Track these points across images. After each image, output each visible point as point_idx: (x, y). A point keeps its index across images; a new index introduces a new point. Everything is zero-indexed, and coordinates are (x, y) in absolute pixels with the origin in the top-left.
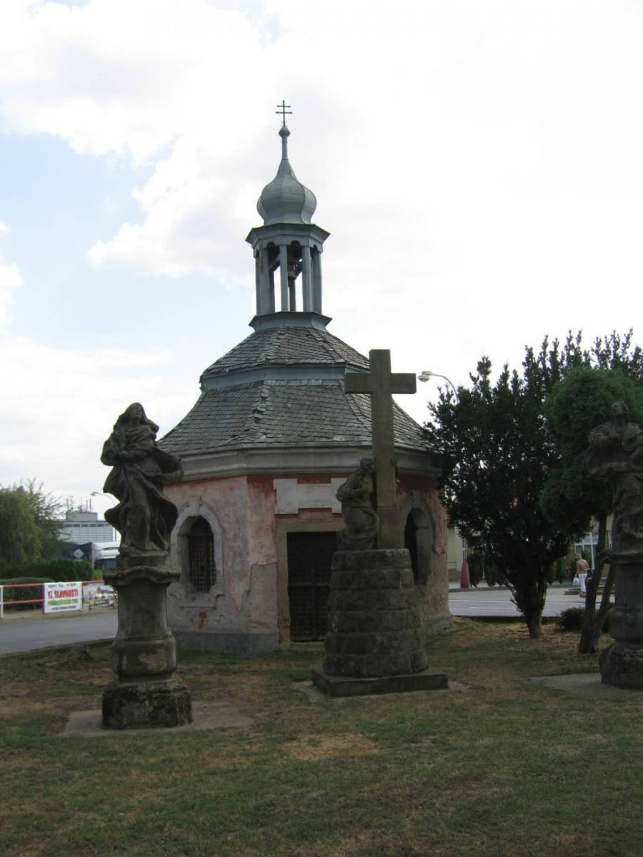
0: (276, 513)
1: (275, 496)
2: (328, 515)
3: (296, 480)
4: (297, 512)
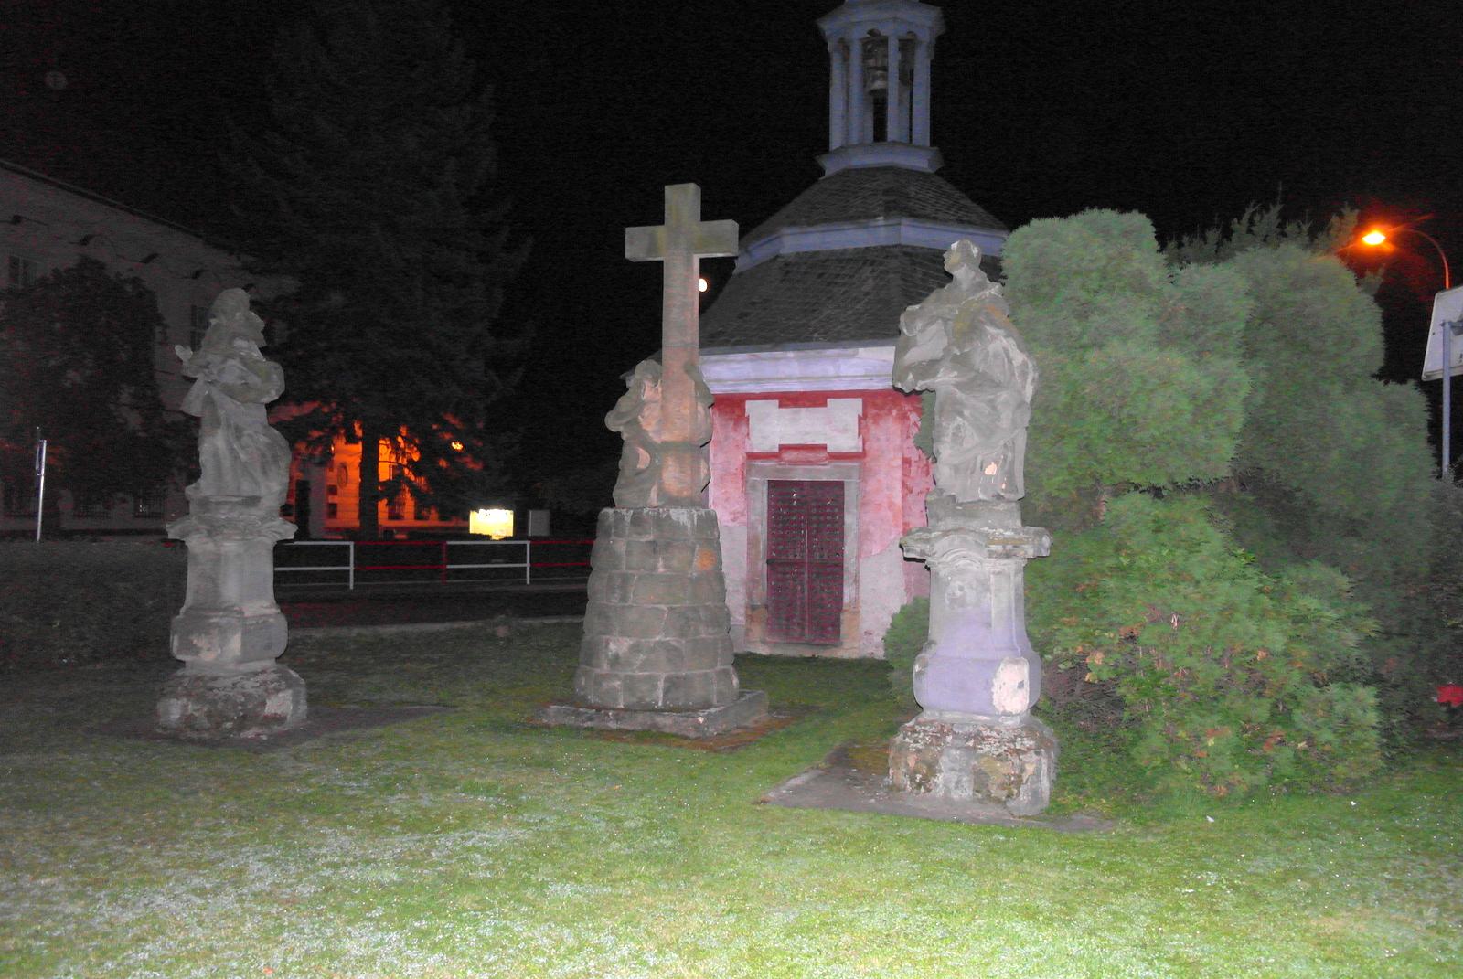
0: (749, 450)
1: (748, 425)
2: (822, 455)
3: (777, 402)
4: (776, 450)
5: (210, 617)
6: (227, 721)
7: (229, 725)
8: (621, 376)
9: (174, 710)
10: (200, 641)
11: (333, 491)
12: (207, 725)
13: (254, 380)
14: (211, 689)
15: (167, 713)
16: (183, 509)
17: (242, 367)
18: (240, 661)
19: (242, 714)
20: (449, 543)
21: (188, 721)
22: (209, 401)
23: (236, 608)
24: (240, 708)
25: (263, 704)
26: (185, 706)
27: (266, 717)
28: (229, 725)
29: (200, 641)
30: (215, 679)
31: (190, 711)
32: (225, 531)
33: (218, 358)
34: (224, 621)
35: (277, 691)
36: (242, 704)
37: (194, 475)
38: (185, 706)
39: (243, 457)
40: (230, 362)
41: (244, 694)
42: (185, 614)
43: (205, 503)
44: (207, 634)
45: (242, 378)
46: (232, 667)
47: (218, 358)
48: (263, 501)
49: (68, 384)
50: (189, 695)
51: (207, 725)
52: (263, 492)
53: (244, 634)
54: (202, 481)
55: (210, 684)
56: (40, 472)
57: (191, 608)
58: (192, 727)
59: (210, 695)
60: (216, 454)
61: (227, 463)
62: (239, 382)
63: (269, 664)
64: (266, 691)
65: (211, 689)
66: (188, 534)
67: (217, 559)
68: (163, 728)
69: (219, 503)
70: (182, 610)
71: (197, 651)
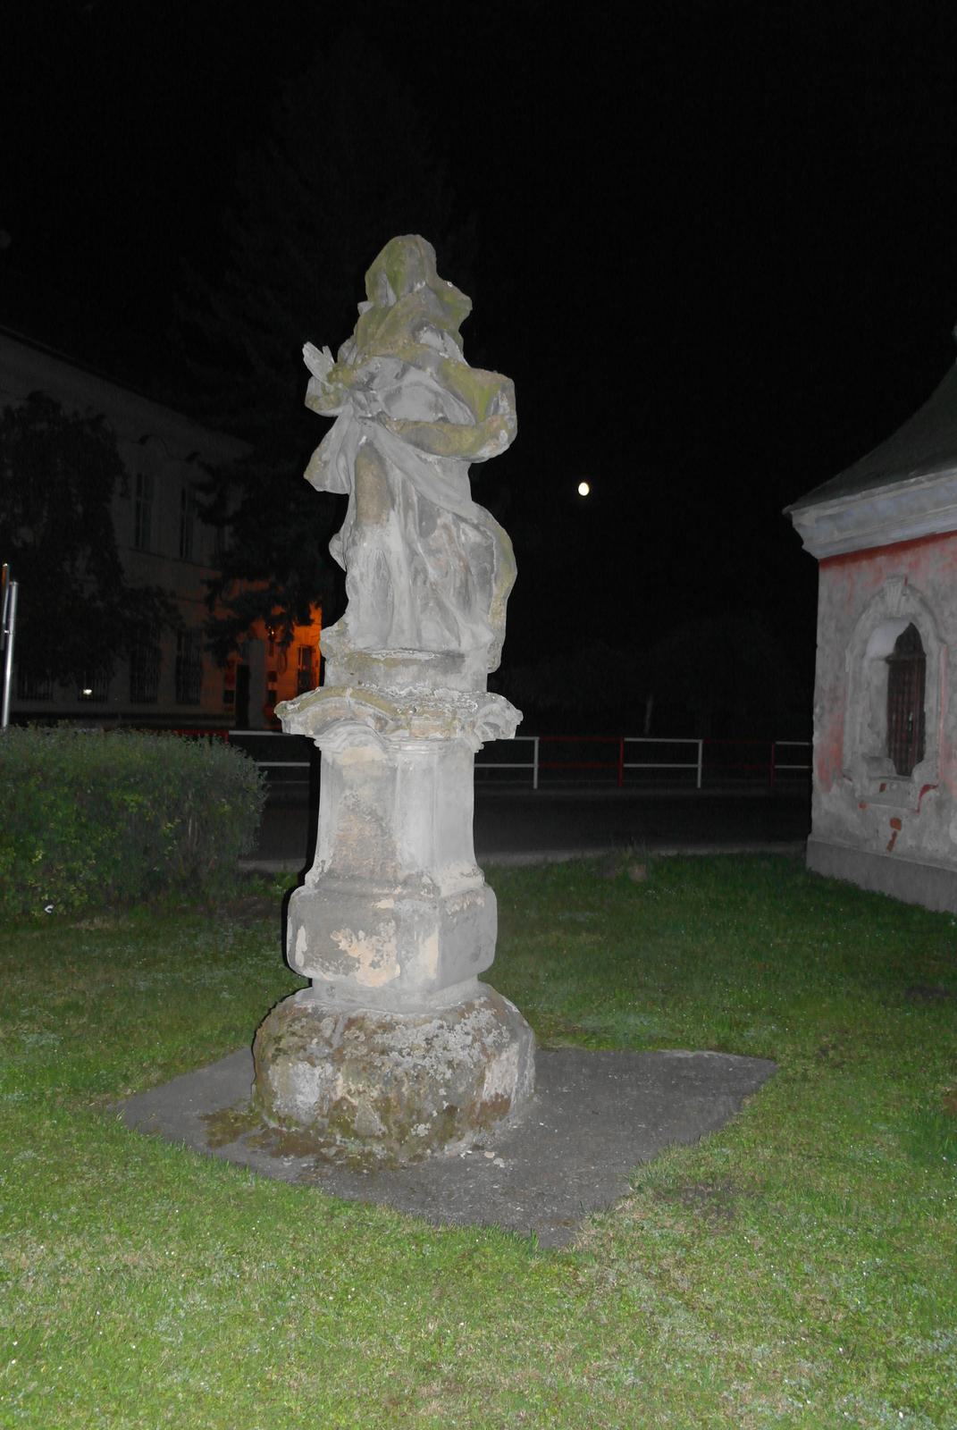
5: (377, 898)
6: (419, 1121)
7: (422, 1129)
8: (785, 510)
9: (304, 1086)
10: (357, 947)
11: (273, 677)
12: (379, 1127)
13: (459, 414)
14: (384, 1051)
15: (292, 1091)
16: (311, 676)
17: (436, 386)
18: (430, 990)
19: (446, 1104)
20: (627, 740)
21: (337, 1114)
22: (370, 453)
23: (426, 880)
24: (442, 1092)
25: (481, 1080)
26: (329, 1083)
27: (484, 1105)
28: (422, 1129)
29: (357, 947)
30: (387, 1027)
31: (340, 1092)
32: (416, 722)
33: (392, 367)
34: (406, 907)
35: (500, 1047)
36: (447, 1085)
37: (335, 607)
38: (329, 1083)
39: (433, 574)
40: (413, 375)
41: (450, 1064)
42: (317, 886)
43: (361, 663)
44: (371, 932)
45: (436, 408)
46: (416, 1000)
47: (392, 367)
48: (468, 661)
49: (19, 544)
50: (337, 1058)
51: (379, 1127)
52: (466, 645)
53: (444, 932)
54: (349, 617)
55: (379, 1039)
56: (7, 628)
57: (330, 874)
58: (346, 1129)
59: (387, 1065)
60: (382, 566)
61: (402, 581)
62: (431, 417)
63: (472, 985)
64: (484, 1050)
65: (384, 1051)
66: (324, 727)
67: (389, 777)
68: (282, 1120)
69: (392, 663)
70: (310, 877)
71: (349, 966)
